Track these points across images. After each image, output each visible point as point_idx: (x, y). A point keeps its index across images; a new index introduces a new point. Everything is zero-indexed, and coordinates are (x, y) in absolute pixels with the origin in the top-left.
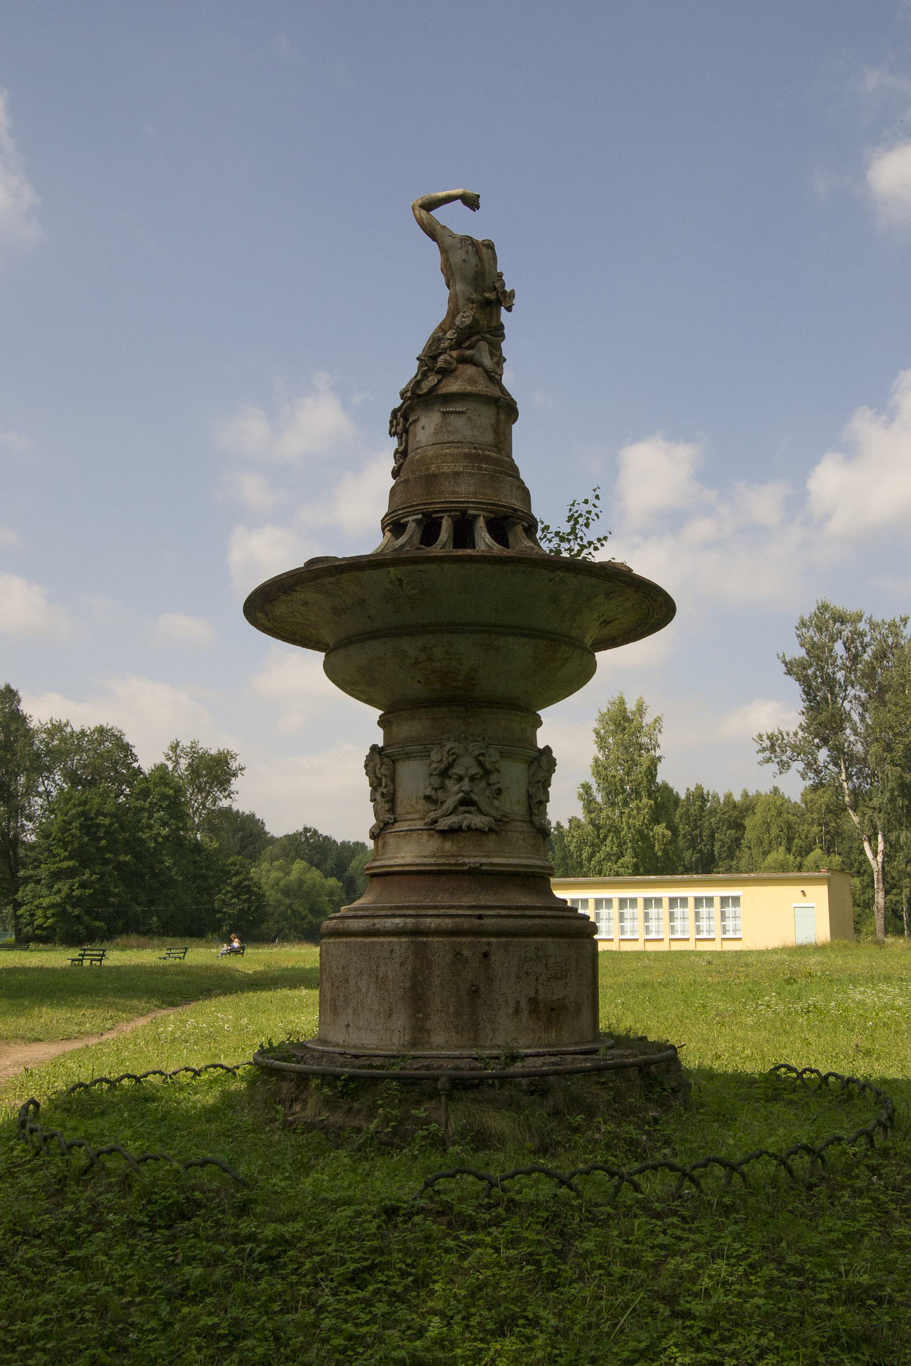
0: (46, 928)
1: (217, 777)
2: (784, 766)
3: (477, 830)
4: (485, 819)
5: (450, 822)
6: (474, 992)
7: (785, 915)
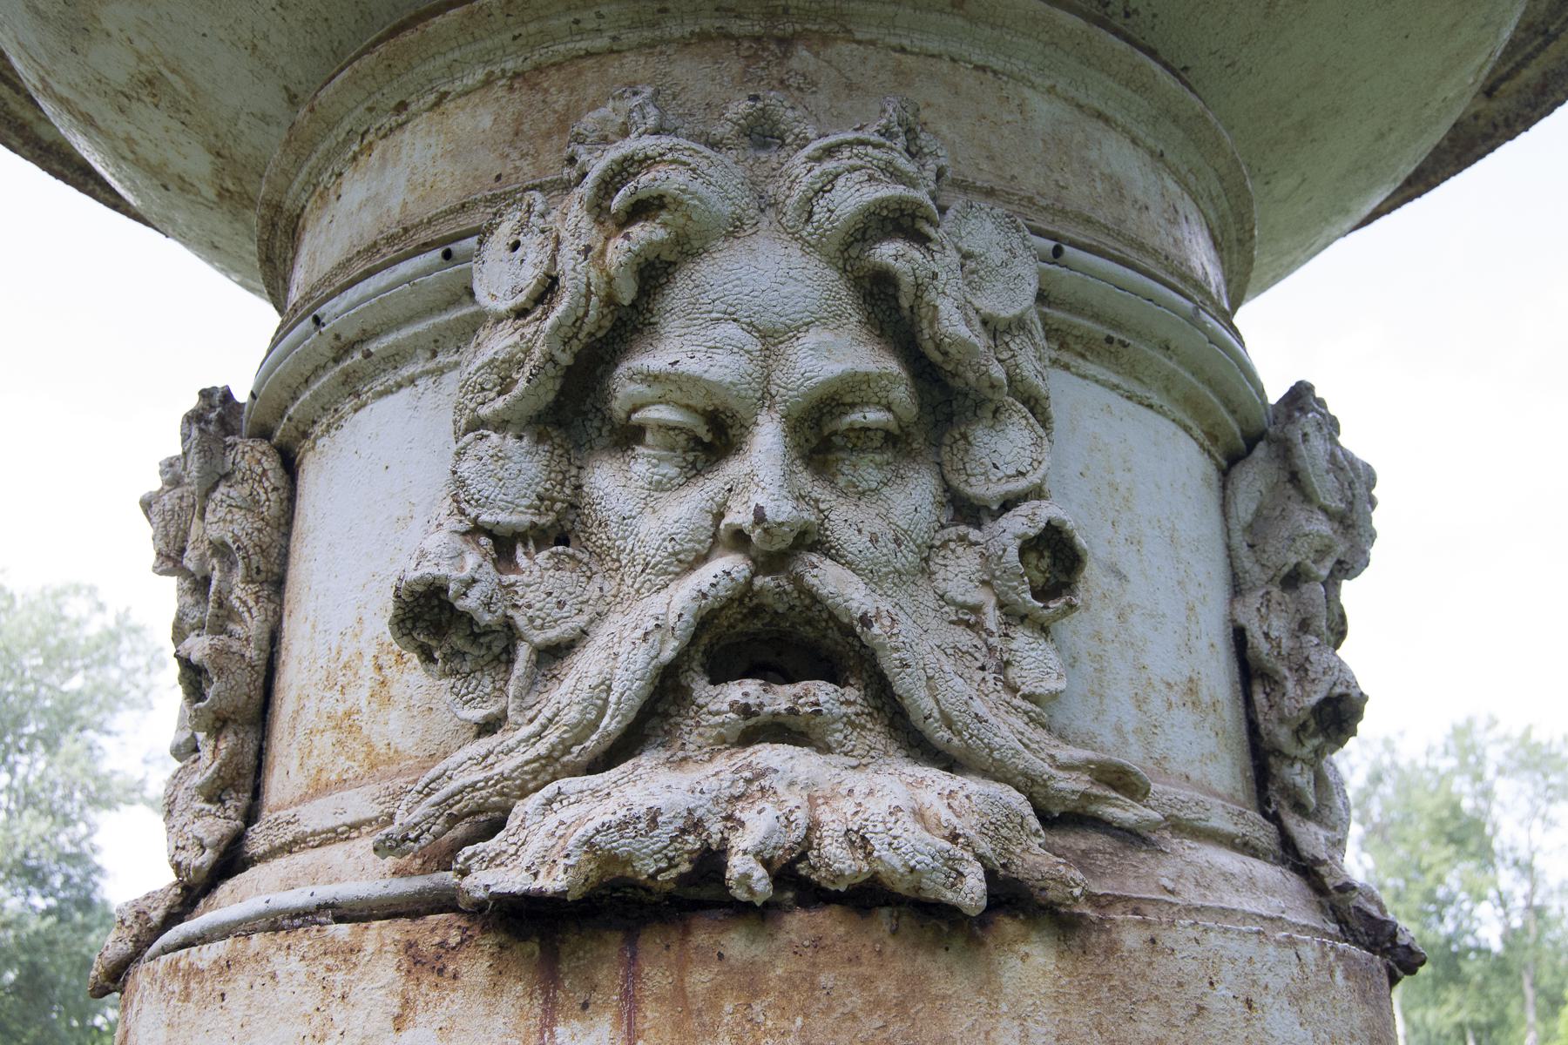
5: (603, 813)
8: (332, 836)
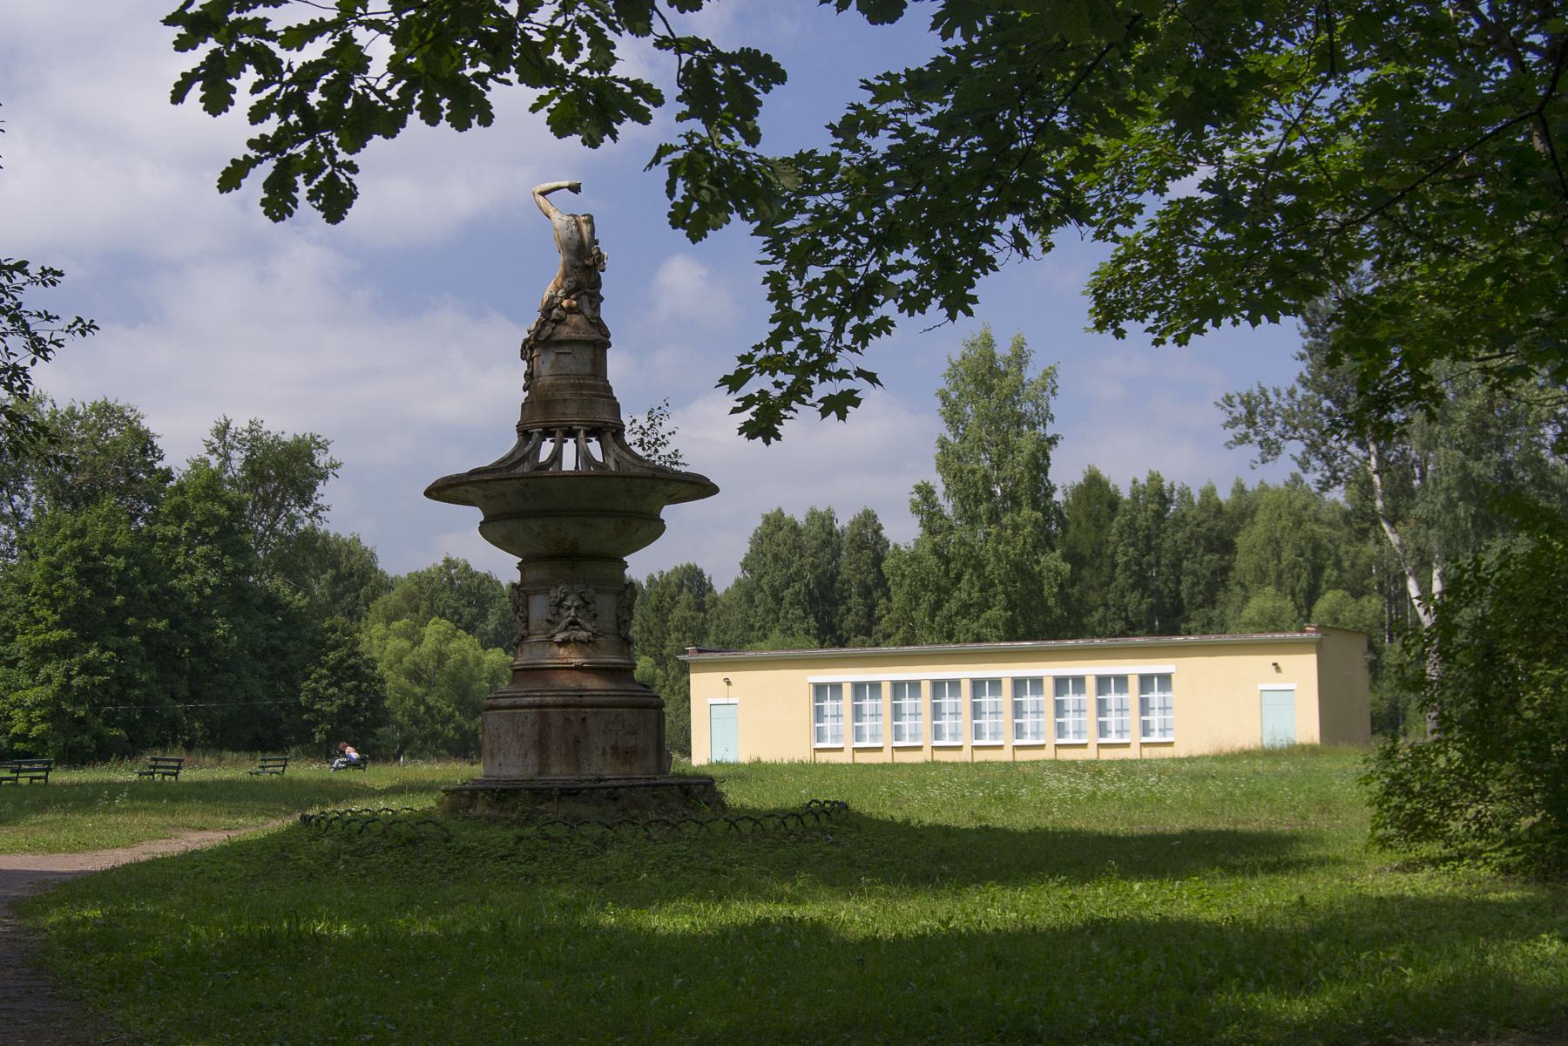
0: (34, 739)
1: (293, 482)
2: (1270, 449)
6: (577, 741)
7: (1244, 702)
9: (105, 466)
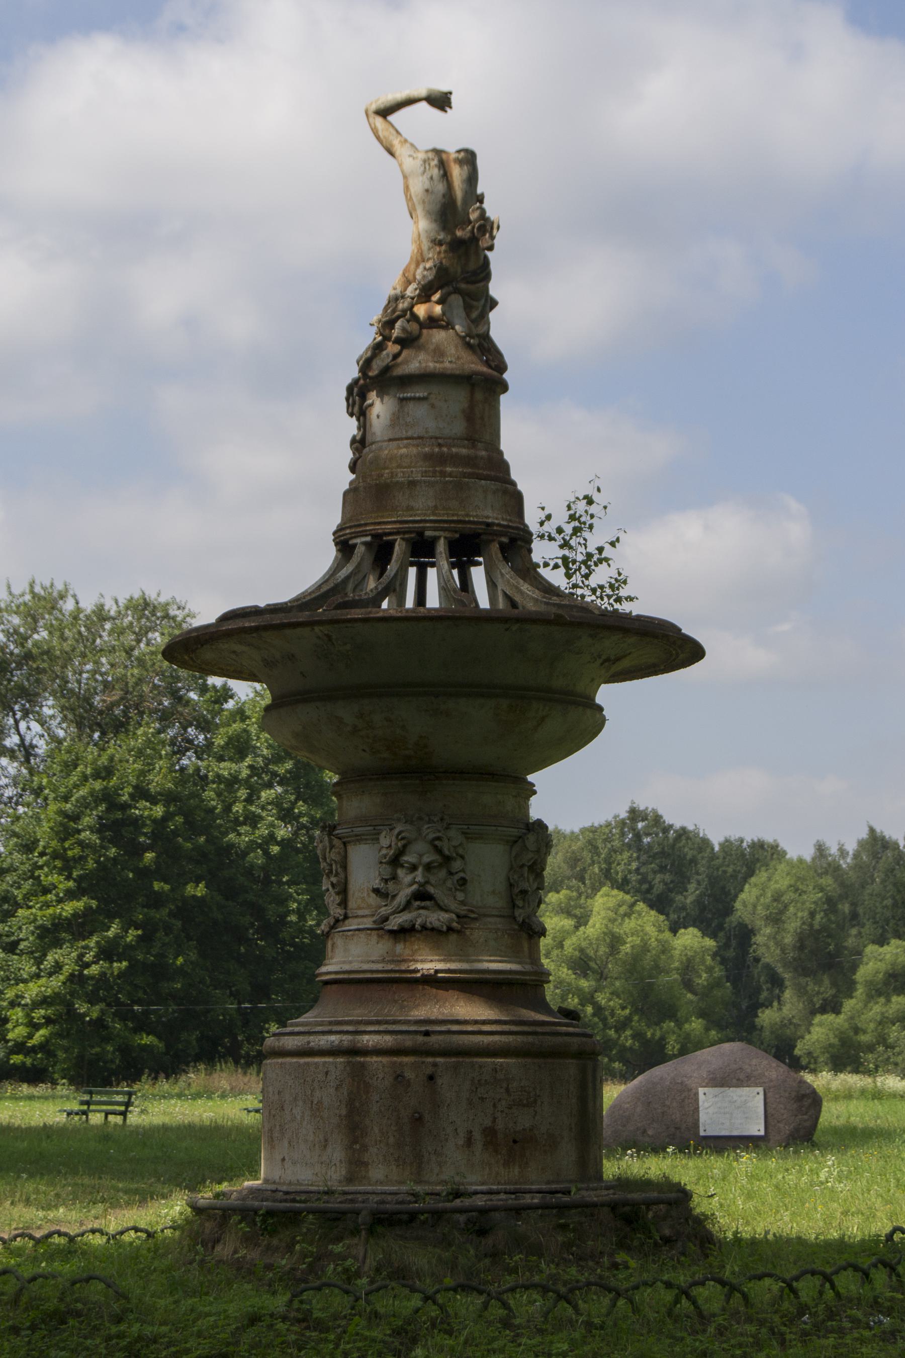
0: (34, 1050)
3: (433, 929)
4: (444, 916)
6: (418, 1120)
8: (363, 916)
9: (140, 681)
